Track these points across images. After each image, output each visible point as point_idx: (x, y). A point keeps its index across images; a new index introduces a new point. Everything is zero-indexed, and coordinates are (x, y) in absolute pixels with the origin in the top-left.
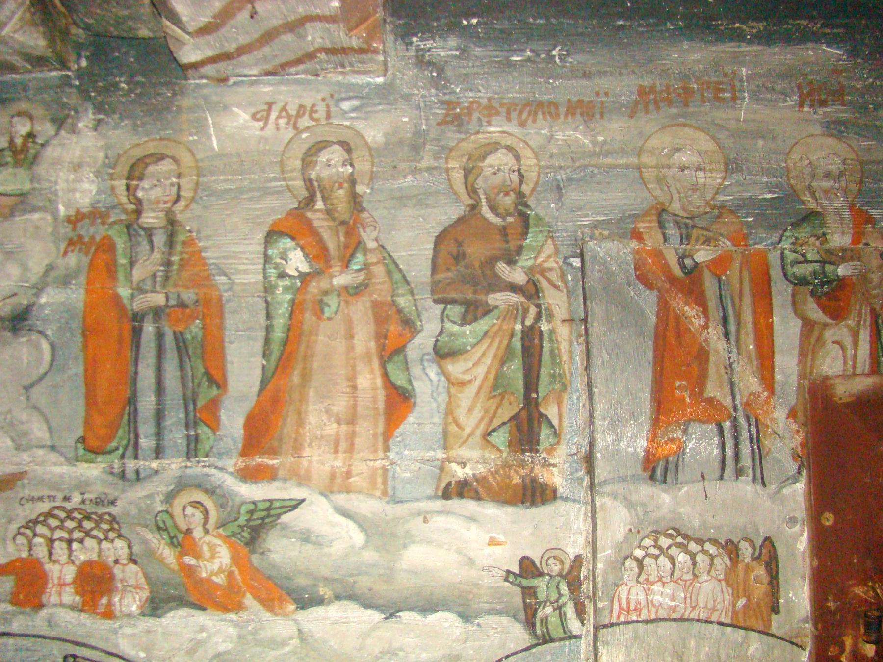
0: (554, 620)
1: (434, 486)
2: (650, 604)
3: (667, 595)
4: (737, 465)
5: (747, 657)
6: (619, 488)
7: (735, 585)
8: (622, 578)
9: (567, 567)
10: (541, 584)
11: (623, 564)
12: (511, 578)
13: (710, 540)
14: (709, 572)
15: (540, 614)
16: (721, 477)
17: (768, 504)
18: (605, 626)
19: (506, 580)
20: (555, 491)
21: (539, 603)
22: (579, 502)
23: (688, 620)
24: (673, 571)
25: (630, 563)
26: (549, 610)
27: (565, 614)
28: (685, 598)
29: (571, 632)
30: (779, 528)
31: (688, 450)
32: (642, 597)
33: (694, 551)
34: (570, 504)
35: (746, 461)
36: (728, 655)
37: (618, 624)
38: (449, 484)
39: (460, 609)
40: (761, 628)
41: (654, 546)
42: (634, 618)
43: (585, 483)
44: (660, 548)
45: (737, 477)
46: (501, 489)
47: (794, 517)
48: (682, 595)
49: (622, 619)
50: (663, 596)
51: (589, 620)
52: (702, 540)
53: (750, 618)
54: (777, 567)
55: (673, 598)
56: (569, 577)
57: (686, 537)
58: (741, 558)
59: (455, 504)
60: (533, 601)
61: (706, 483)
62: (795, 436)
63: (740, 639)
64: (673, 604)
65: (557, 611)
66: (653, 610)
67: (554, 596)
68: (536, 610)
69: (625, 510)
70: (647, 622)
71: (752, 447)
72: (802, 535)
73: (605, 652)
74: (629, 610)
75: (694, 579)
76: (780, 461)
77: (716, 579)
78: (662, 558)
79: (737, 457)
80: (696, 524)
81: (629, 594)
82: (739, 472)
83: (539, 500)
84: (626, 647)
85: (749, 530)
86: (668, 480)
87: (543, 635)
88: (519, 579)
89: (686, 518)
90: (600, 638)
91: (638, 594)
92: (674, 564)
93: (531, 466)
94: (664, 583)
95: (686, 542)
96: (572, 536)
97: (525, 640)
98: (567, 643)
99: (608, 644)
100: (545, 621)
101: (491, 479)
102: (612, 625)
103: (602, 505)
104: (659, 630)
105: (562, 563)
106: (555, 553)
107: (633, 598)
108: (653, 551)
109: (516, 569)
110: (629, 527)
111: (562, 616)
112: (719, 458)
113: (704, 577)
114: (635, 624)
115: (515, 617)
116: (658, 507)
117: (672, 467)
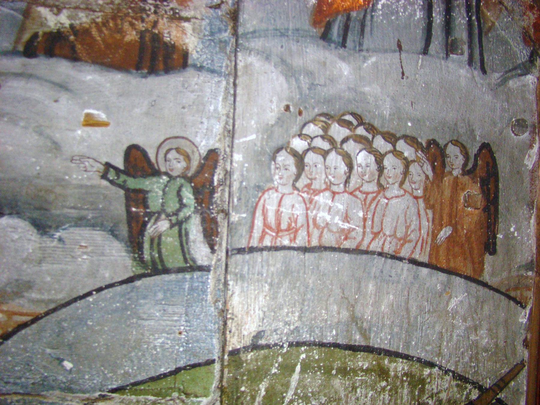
0: (170, 241)
1: (13, 38)
2: (311, 223)
3: (337, 212)
4: (447, 38)
5: (447, 312)
6: (275, 45)
7: (438, 207)
8: (272, 180)
9: (195, 164)
10: (155, 187)
11: (274, 158)
12: (112, 175)
13: (405, 137)
14: (402, 183)
15: (150, 230)
16: (425, 51)
17: (488, 97)
18: (240, 251)
19: (104, 176)
20: (185, 55)
21: (150, 215)
22: (220, 74)
23: (366, 252)
24: (349, 177)
25: (283, 157)
26: (163, 225)
27: (187, 234)
28: (365, 220)
29: (194, 261)
30: (501, 133)
31: (379, 7)
32: (299, 211)
33: (382, 151)
34: (204, 76)
35: (461, 33)
36: (421, 309)
37: (262, 250)
38: (35, 36)
39: (36, 214)
40: (469, 272)
41: (323, 137)
42: (286, 242)
43: (228, 49)
44: (332, 141)
45: (447, 55)
46: (108, 46)
47: (524, 121)
48: (361, 214)
49: (267, 242)
50: (332, 213)
51: (220, 244)
52: (393, 135)
53: (455, 256)
54: (497, 187)
55: (346, 218)
56: (199, 179)
57: (371, 128)
58: (447, 169)
59: (41, 65)
60: (141, 211)
61: (403, 55)
62: (528, 13)
63: (439, 287)
64: (346, 226)
65: (176, 229)
66: (316, 233)
67: (172, 206)
68: (145, 224)
69: (282, 79)
70: (305, 250)
71: (470, 18)
72: (531, 147)
73: (237, 290)
74: (278, 230)
75: (378, 193)
76: (506, 43)
77: (411, 194)
78: (333, 155)
79: (448, 26)
80: (387, 113)
81: (279, 205)
82: (450, 48)
83: (161, 66)
84: (271, 285)
85: (462, 131)
86: (349, 43)
87: (153, 261)
88: (123, 177)
89: (371, 99)
90: (231, 269)
91: (293, 207)
92: (350, 167)
93: (152, 17)
94: (334, 193)
95: (370, 137)
96: (205, 120)
97: (126, 267)
98: (188, 276)
99: (242, 277)
100: (157, 241)
101: (94, 32)
102: (251, 250)
103: (246, 67)
104: (323, 263)
105: (188, 158)
106: (178, 145)
107: (285, 210)
108: (319, 143)
109: (119, 163)
110: (285, 103)
111: (183, 237)
112: (423, 24)
113: (395, 191)
114: (286, 252)
115: (114, 233)
116: (332, 80)
117: (355, 26)
